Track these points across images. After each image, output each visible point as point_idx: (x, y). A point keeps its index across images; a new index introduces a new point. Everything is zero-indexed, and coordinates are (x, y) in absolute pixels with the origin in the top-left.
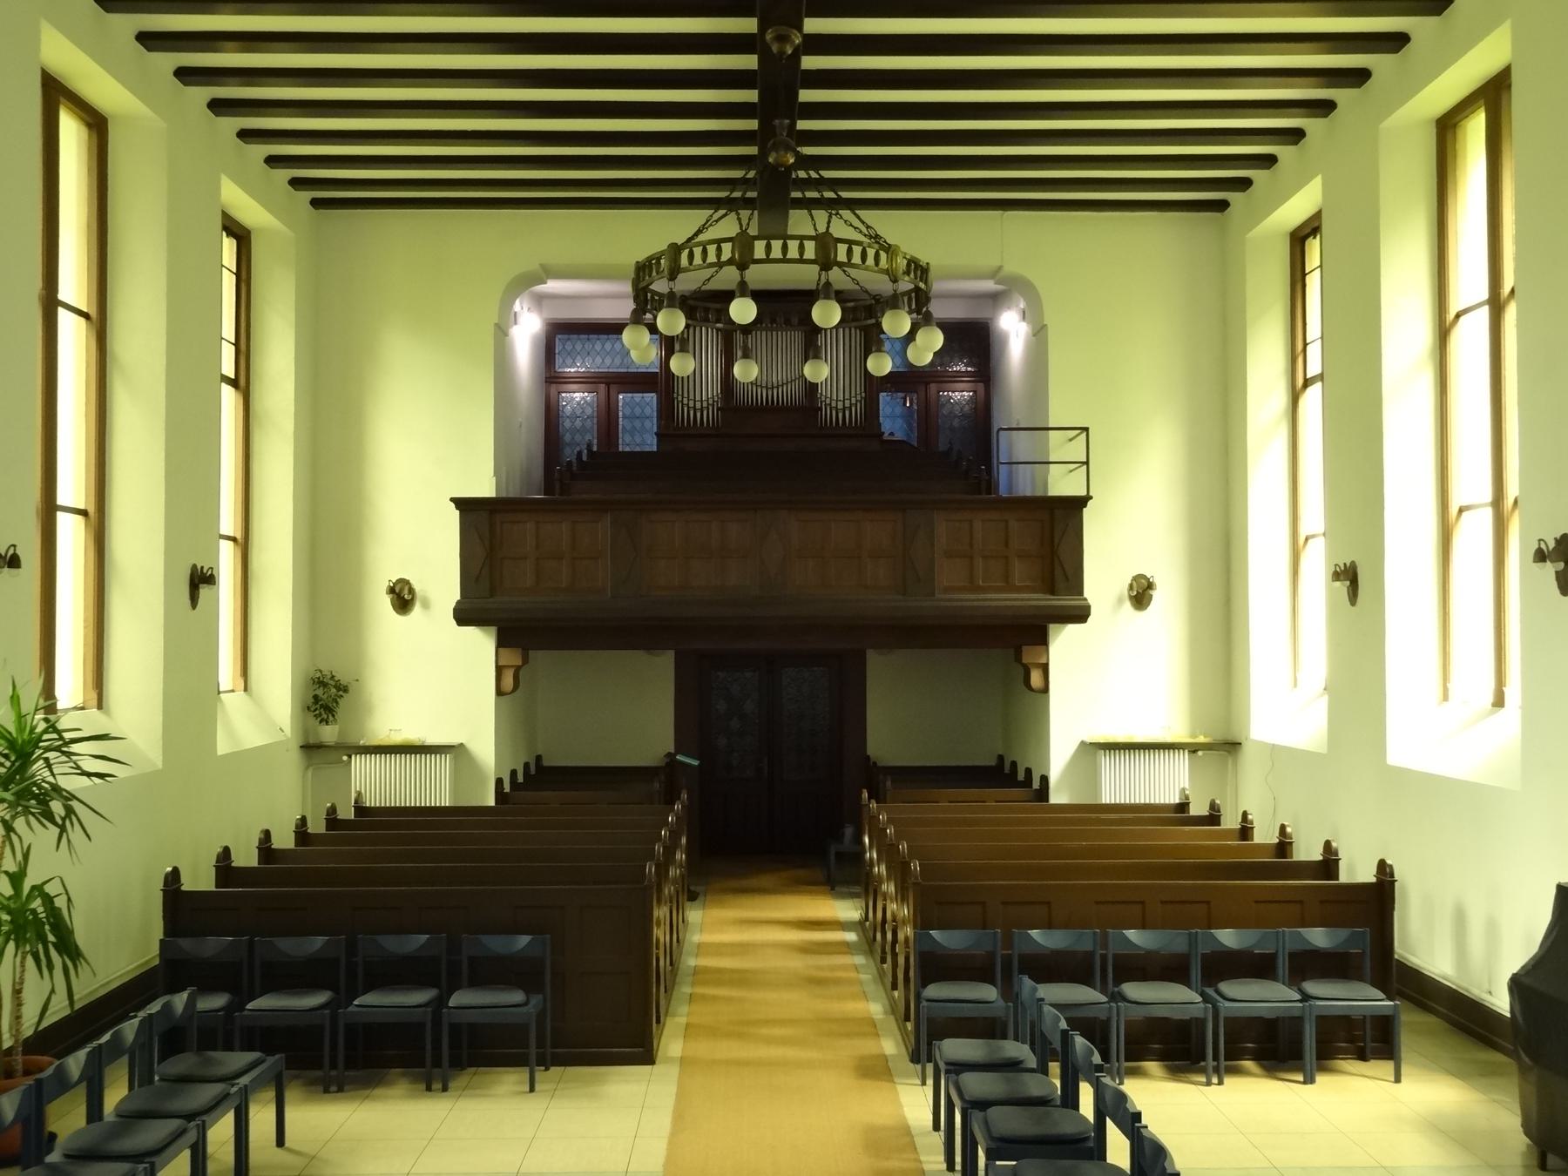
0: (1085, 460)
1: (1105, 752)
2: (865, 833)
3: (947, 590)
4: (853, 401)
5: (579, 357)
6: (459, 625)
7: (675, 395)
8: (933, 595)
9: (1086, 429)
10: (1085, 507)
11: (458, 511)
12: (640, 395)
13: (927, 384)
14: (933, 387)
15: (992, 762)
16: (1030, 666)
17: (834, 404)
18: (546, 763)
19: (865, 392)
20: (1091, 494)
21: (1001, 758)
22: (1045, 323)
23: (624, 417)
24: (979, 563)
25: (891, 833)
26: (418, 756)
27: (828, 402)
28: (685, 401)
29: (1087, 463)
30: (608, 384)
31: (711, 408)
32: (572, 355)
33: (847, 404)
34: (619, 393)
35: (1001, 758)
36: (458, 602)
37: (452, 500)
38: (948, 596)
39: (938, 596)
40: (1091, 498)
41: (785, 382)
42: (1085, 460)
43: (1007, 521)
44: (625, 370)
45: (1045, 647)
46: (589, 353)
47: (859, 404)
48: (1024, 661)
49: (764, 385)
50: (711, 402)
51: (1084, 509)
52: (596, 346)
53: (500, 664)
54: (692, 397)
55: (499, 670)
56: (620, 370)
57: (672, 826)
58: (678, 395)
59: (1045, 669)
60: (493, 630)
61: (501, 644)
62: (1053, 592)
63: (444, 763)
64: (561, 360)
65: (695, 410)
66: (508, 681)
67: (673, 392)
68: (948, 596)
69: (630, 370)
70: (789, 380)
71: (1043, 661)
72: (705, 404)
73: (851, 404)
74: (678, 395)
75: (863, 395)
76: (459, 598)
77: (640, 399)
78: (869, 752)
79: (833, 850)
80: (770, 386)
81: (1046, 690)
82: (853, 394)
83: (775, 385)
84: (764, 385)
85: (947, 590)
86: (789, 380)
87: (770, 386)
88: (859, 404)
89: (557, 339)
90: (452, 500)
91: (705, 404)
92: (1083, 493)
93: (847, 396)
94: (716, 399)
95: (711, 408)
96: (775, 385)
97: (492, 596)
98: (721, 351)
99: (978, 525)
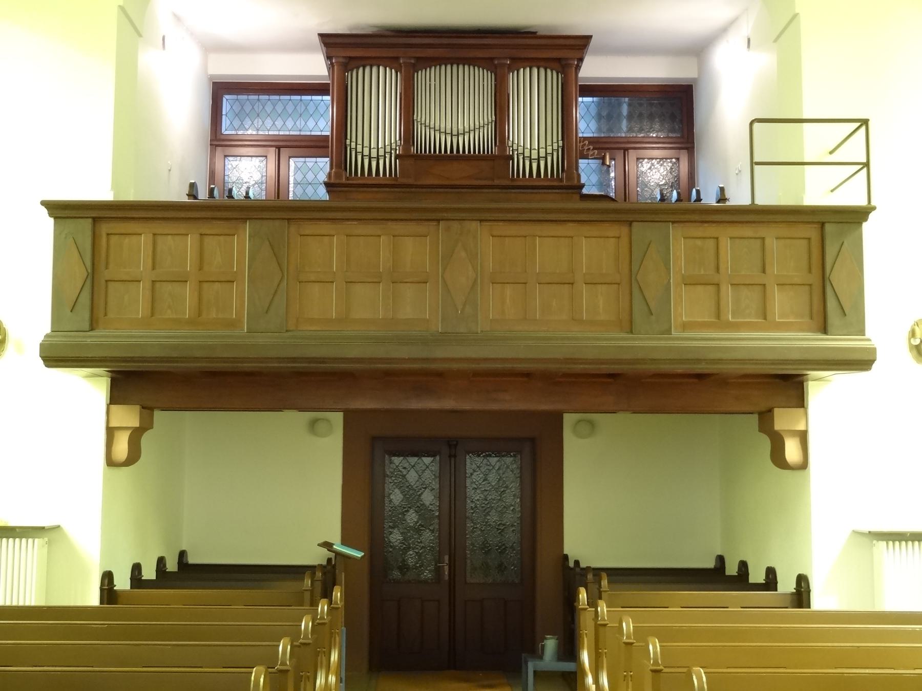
0: (864, 160)
1: (887, 543)
2: (583, 648)
3: (685, 326)
4: (549, 150)
5: (247, 119)
6: (47, 366)
7: (348, 142)
8: (669, 331)
9: (865, 122)
10: (866, 220)
11: (52, 220)
12: (314, 159)
13: (626, 150)
14: (632, 154)
15: (710, 564)
16: (783, 434)
17: (527, 154)
18: (192, 560)
19: (563, 139)
20: (873, 203)
21: (721, 559)
22: (797, 11)
23: (296, 184)
24: (728, 292)
25: (655, 653)
26: (24, 540)
27: (521, 150)
28: (359, 148)
29: (867, 165)
30: (279, 148)
31: (388, 156)
32: (240, 115)
33: (542, 154)
34: (290, 157)
35: (721, 559)
36: (47, 336)
37: (44, 203)
38: (686, 335)
39: (674, 333)
40: (874, 208)
41: (472, 128)
42: (864, 160)
43: (763, 239)
44: (297, 133)
45: (802, 409)
46: (258, 116)
47: (555, 154)
48: (777, 427)
49: (449, 131)
50: (388, 150)
51: (865, 225)
52: (266, 108)
53: (112, 425)
54: (366, 143)
55: (111, 432)
56: (292, 133)
57: (306, 637)
58: (351, 142)
59: (803, 437)
60: (138, 408)
61: (116, 397)
62: (825, 331)
63: (35, 548)
64: (228, 122)
65: (370, 158)
66: (122, 448)
67: (346, 138)
68: (686, 335)
69: (303, 133)
70: (477, 126)
71: (801, 427)
72: (381, 152)
73: (546, 153)
74: (351, 142)
75: (561, 143)
76: (48, 330)
77: (312, 164)
78: (567, 550)
79: (531, 666)
80: (455, 133)
81: (804, 465)
82: (549, 143)
83: (461, 131)
84: (449, 131)
85: (685, 326)
86: (477, 126)
87: (455, 133)
88: (555, 154)
89: (224, 100)
90: (44, 203)
91: (381, 152)
92: (862, 202)
93: (542, 144)
94: (394, 146)
95: (388, 156)
96: (461, 131)
97: (92, 329)
98: (401, 94)
99: (726, 245)
